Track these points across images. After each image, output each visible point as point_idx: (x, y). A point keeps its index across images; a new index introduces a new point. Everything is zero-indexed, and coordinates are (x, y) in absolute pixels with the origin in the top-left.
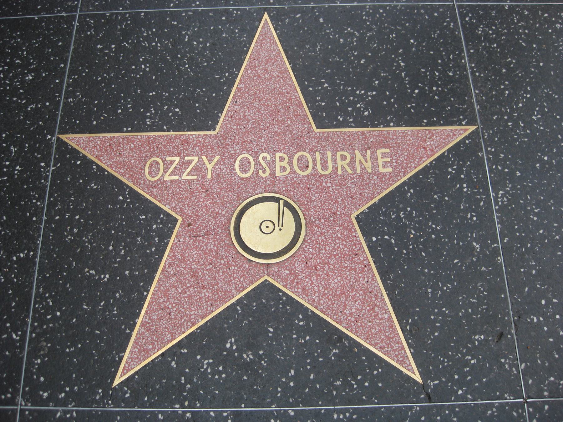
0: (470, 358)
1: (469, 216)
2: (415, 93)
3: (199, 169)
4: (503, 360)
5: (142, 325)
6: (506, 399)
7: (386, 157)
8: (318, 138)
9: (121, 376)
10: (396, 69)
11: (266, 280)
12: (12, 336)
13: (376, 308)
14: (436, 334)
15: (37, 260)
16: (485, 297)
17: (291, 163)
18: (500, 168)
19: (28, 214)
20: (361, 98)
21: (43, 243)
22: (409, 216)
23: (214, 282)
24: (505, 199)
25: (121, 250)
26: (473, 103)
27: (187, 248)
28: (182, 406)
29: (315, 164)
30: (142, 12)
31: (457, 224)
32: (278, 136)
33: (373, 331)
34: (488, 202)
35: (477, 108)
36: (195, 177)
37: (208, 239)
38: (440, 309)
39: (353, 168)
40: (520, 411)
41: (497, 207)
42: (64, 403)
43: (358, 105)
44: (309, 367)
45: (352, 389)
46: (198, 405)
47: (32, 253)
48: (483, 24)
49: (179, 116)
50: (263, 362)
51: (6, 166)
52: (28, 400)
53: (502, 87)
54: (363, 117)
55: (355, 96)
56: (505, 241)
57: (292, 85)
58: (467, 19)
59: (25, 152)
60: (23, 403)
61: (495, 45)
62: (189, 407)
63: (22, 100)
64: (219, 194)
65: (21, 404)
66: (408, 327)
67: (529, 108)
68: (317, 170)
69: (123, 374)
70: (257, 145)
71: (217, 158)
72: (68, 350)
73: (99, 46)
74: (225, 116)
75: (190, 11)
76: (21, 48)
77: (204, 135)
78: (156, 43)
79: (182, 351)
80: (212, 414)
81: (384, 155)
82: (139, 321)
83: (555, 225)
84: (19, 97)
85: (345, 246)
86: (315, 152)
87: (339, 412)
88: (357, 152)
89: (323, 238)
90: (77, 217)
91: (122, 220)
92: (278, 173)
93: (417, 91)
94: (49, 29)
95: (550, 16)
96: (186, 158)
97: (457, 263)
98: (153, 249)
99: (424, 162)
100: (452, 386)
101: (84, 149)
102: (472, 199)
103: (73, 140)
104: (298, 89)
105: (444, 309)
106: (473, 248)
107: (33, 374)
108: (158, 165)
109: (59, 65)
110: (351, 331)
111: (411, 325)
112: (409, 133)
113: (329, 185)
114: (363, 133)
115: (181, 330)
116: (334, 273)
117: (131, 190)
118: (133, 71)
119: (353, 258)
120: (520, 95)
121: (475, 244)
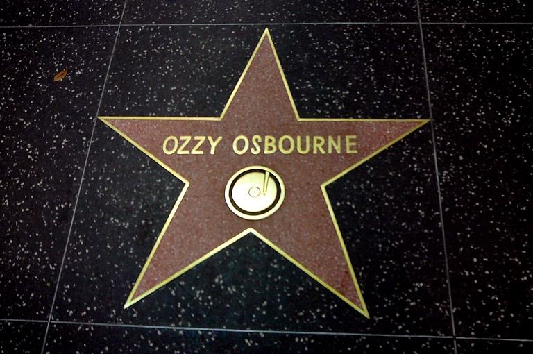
1: (417, 190)
3: (206, 146)
4: (437, 304)
6: (439, 335)
7: (345, 143)
10: (367, 74)
17: (277, 144)
24: (449, 177)
25: (140, 205)
26: (427, 103)
28: (177, 325)
29: (296, 145)
34: (434, 178)
35: (431, 105)
40: (450, 346)
42: (85, 319)
45: (312, 319)
47: (70, 205)
48: (442, 40)
52: (57, 317)
60: (53, 319)
62: (183, 326)
65: (51, 320)
67: (475, 106)
71: (220, 138)
73: (134, 51)
81: (351, 140)
93: (382, 92)
95: (501, 33)
100: (393, 322)
102: (420, 177)
111: (363, 271)
120: (468, 96)
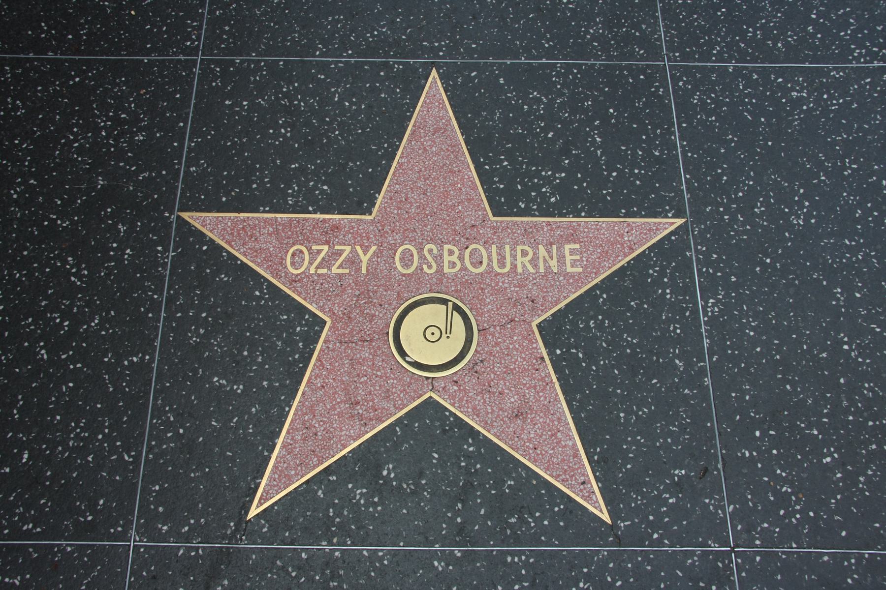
0: (668, 496)
1: (671, 329)
2: (612, 176)
3: (353, 262)
4: (707, 501)
5: (283, 446)
7: (571, 255)
8: (494, 228)
9: (258, 507)
10: (591, 146)
11: (431, 397)
13: (559, 434)
14: (629, 466)
15: (155, 365)
17: (461, 258)
18: (711, 271)
19: (142, 309)
20: (548, 181)
22: (600, 326)
23: (369, 397)
24: (716, 309)
27: (337, 355)
28: (330, 543)
29: (490, 259)
30: (280, 60)
32: (447, 224)
33: (555, 460)
34: (695, 312)
35: (687, 196)
36: (347, 271)
37: (363, 346)
38: (634, 438)
39: (536, 266)
41: (706, 319)
42: (187, 538)
43: (544, 190)
44: (479, 501)
46: (349, 543)
47: (147, 357)
49: (327, 194)
50: (425, 493)
51: (113, 249)
53: (719, 171)
54: (549, 205)
55: (541, 178)
56: (714, 359)
57: (464, 162)
58: (681, 84)
59: (137, 232)
60: (138, 539)
61: (714, 118)
64: (376, 292)
65: (134, 539)
66: (596, 458)
68: (492, 267)
69: (260, 504)
70: (422, 235)
71: (374, 248)
72: (192, 475)
73: (227, 102)
74: (384, 198)
75: (341, 62)
76: (128, 99)
77: (358, 220)
78: (299, 101)
79: (331, 478)
80: (365, 553)
81: (572, 252)
82: (280, 442)
83: (776, 342)
84: (127, 161)
85: (524, 359)
86: (490, 246)
87: (513, 554)
88: (541, 247)
89: (498, 349)
90: (204, 315)
91: (260, 320)
92: (446, 270)
93: (614, 174)
94: (163, 77)
95: (786, 81)
96: (337, 247)
97: (656, 383)
98: (297, 356)
99: (620, 261)
101: (211, 231)
103: (195, 219)
104: (472, 167)
105: (639, 438)
106: (676, 367)
108: (293, 252)
109: (178, 124)
110: (529, 460)
112: (604, 225)
113: (506, 285)
114: (548, 224)
115: (329, 454)
116: (511, 390)
117: (270, 284)
118: (271, 136)
119: (533, 374)
121: (677, 361)
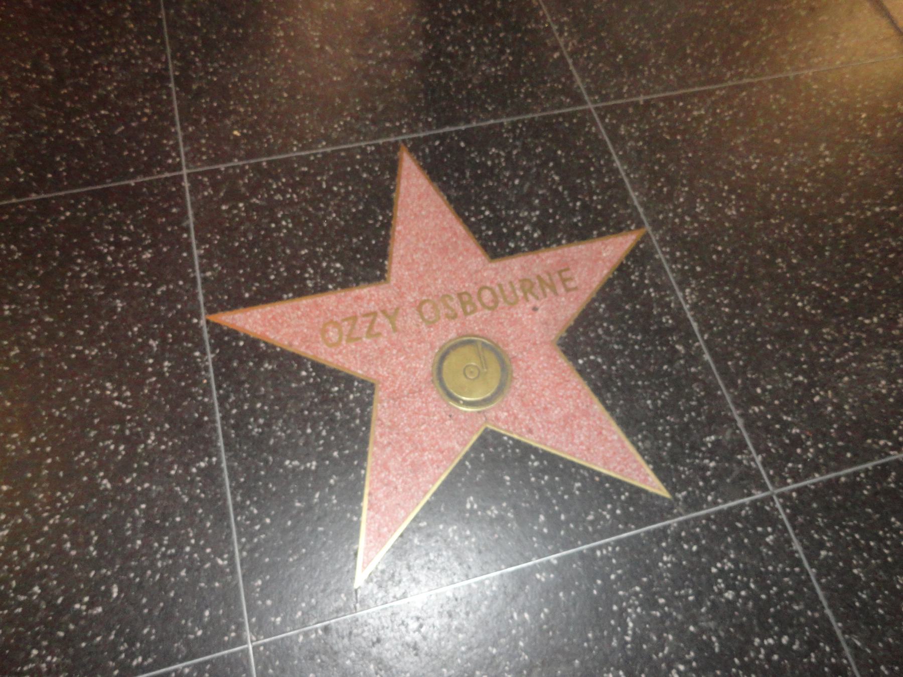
12: (217, 564)
15: (224, 465)
16: (703, 397)
21: (226, 445)
22: (607, 331)
23: (434, 442)
31: (655, 331)
54: (534, 240)
63: (146, 283)
76: (125, 223)
84: (141, 280)
87: (600, 547)
107: (256, 600)
